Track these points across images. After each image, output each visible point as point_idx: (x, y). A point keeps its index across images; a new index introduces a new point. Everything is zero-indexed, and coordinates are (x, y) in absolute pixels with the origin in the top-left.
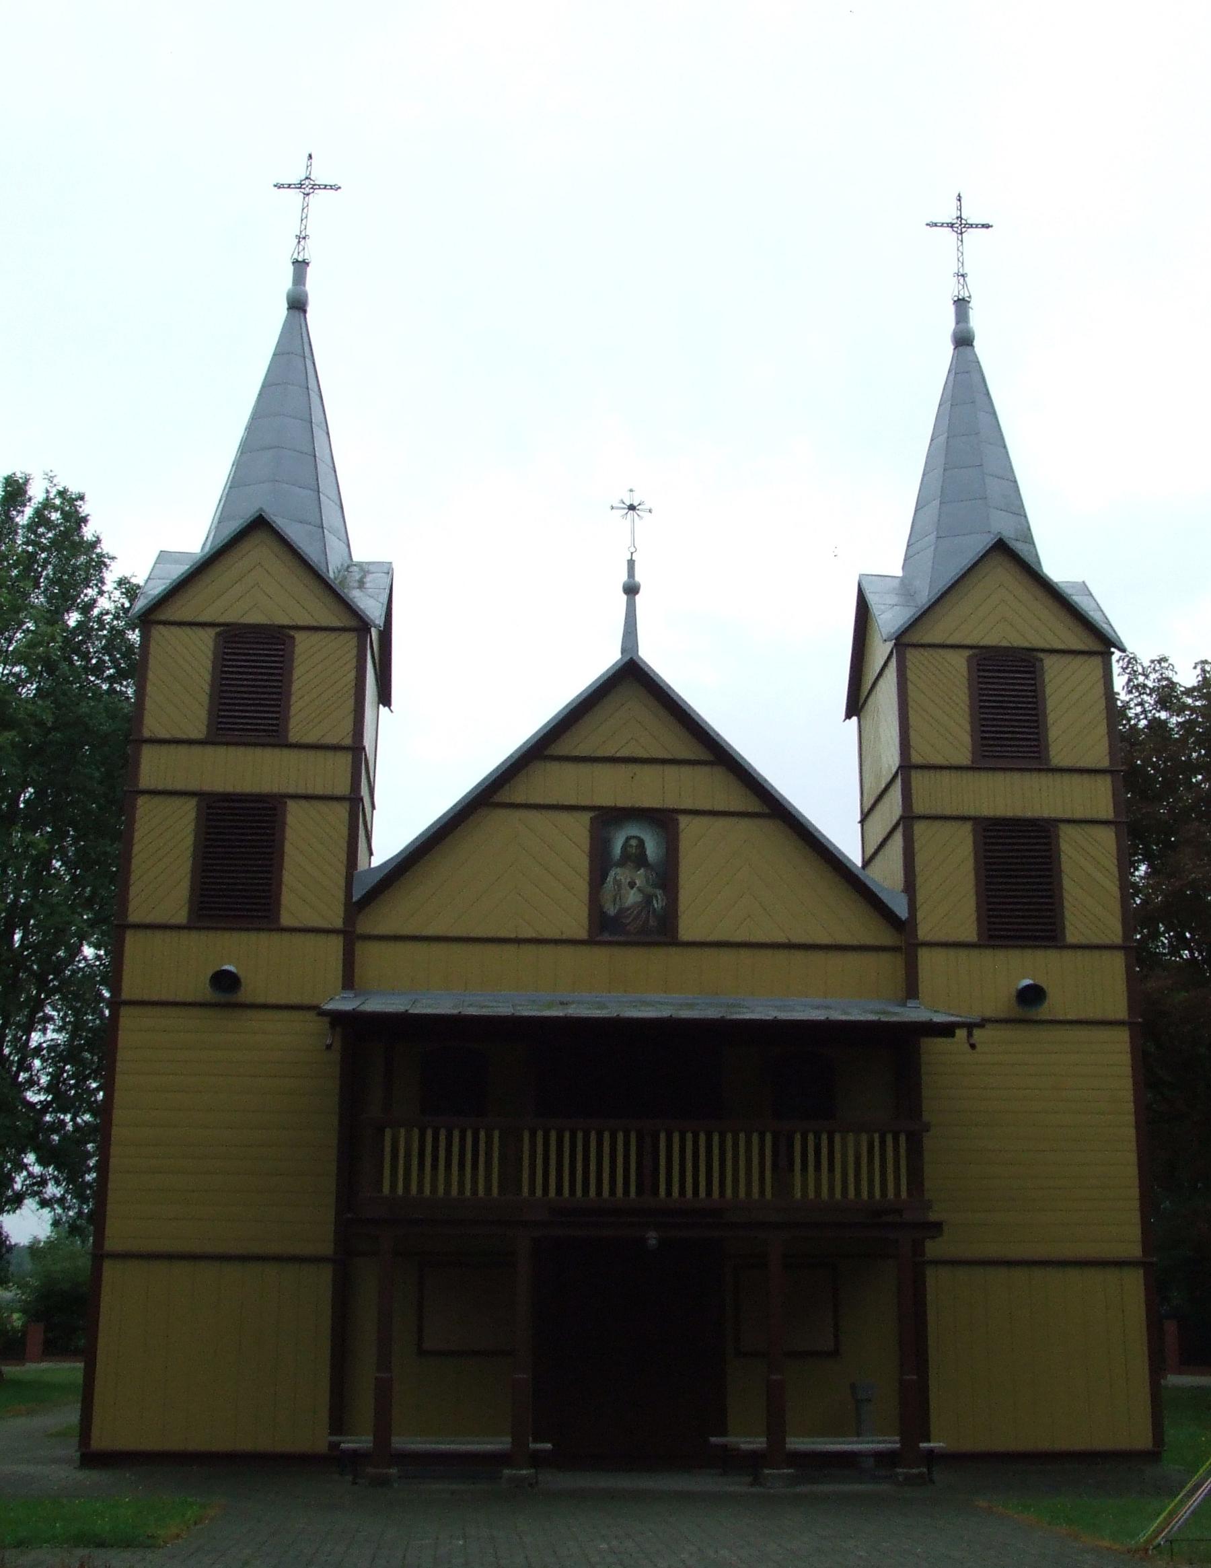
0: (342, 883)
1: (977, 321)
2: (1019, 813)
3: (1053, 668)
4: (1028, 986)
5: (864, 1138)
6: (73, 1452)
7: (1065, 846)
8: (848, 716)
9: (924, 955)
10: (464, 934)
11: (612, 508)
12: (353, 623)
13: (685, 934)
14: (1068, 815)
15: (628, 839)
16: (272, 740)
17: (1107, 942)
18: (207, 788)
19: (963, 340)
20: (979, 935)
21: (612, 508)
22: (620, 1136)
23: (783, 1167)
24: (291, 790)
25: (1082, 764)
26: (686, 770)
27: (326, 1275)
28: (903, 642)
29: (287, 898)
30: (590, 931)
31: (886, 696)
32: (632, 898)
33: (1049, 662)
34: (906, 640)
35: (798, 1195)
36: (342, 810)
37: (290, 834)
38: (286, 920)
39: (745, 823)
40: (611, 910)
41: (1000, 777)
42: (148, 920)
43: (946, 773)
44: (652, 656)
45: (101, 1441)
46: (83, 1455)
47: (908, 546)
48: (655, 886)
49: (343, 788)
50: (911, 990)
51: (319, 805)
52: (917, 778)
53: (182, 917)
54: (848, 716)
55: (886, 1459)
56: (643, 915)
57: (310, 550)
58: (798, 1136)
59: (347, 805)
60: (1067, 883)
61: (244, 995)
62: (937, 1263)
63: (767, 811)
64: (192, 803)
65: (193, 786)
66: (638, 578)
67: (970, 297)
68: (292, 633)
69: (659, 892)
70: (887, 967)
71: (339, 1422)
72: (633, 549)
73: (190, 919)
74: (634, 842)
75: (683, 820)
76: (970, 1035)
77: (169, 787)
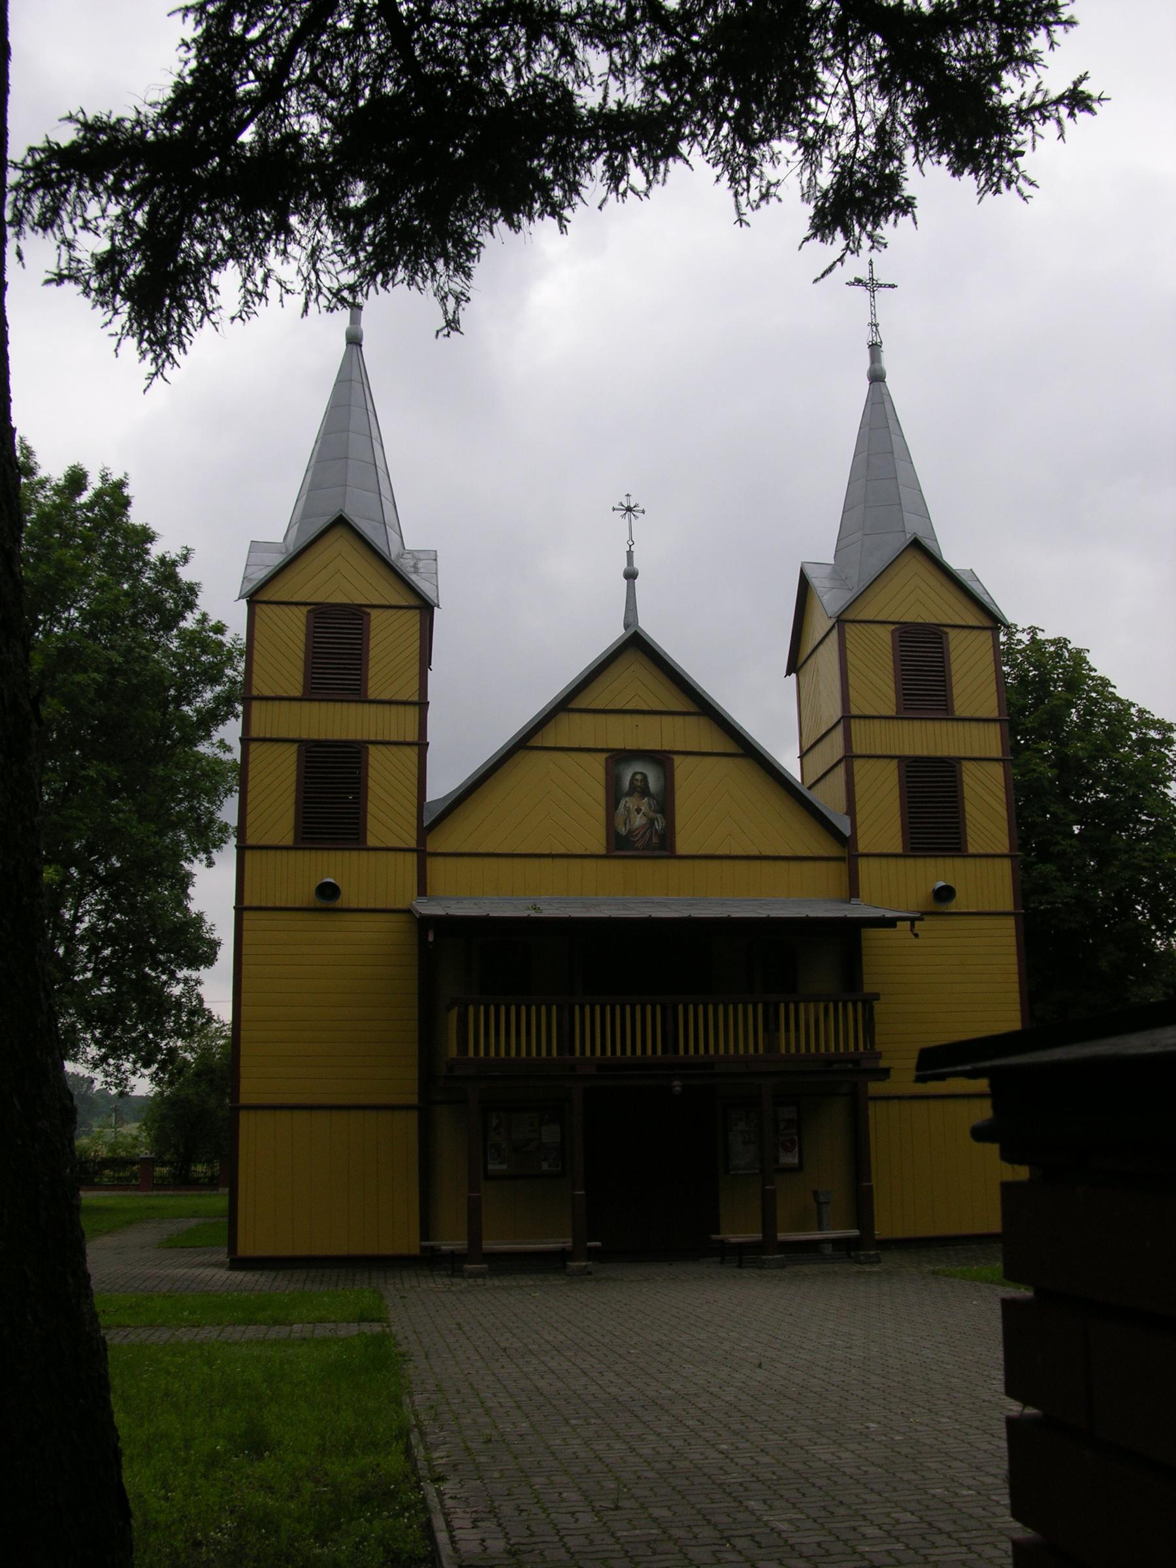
0: (415, 811)
1: (888, 362)
2: (932, 753)
3: (955, 639)
4: (943, 887)
5: (822, 1005)
6: (223, 1257)
7: (966, 778)
8: (788, 673)
9: (863, 863)
10: (510, 852)
11: (614, 509)
12: (413, 601)
13: (682, 848)
14: (969, 755)
15: (635, 774)
16: (357, 698)
17: (999, 852)
18: (304, 736)
19: (877, 377)
20: (904, 847)
21: (614, 509)
22: (649, 1008)
23: (771, 1027)
24: (372, 738)
25: (978, 715)
26: (679, 720)
27: (413, 1118)
28: (841, 622)
29: (372, 824)
30: (607, 849)
31: (826, 661)
32: (639, 821)
33: (952, 634)
34: (844, 617)
35: (783, 1051)
36: (413, 753)
37: (371, 772)
38: (371, 841)
39: (724, 761)
40: (623, 831)
41: (917, 724)
42: (262, 843)
43: (877, 722)
44: (650, 626)
45: (246, 1248)
46: (232, 1261)
47: (838, 540)
48: (656, 811)
49: (412, 736)
50: (853, 891)
51: (394, 749)
52: (855, 725)
53: (289, 840)
54: (788, 673)
55: (841, 1245)
56: (648, 834)
57: (378, 541)
58: (782, 1005)
59: (416, 749)
60: (969, 808)
61: (341, 902)
62: (875, 1098)
63: (741, 751)
64: (295, 747)
65: (293, 735)
66: (637, 564)
67: (881, 342)
68: (368, 610)
69: (659, 816)
70: (831, 875)
71: (426, 1230)
72: (631, 543)
73: (296, 840)
74: (639, 777)
75: (677, 760)
76: (912, 926)
77: (275, 736)
